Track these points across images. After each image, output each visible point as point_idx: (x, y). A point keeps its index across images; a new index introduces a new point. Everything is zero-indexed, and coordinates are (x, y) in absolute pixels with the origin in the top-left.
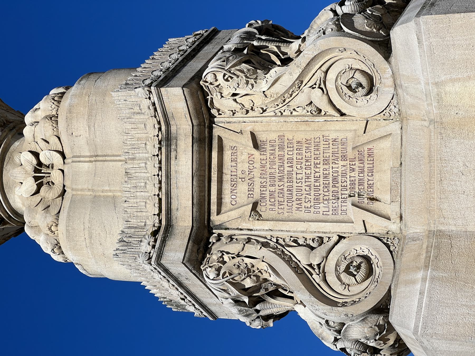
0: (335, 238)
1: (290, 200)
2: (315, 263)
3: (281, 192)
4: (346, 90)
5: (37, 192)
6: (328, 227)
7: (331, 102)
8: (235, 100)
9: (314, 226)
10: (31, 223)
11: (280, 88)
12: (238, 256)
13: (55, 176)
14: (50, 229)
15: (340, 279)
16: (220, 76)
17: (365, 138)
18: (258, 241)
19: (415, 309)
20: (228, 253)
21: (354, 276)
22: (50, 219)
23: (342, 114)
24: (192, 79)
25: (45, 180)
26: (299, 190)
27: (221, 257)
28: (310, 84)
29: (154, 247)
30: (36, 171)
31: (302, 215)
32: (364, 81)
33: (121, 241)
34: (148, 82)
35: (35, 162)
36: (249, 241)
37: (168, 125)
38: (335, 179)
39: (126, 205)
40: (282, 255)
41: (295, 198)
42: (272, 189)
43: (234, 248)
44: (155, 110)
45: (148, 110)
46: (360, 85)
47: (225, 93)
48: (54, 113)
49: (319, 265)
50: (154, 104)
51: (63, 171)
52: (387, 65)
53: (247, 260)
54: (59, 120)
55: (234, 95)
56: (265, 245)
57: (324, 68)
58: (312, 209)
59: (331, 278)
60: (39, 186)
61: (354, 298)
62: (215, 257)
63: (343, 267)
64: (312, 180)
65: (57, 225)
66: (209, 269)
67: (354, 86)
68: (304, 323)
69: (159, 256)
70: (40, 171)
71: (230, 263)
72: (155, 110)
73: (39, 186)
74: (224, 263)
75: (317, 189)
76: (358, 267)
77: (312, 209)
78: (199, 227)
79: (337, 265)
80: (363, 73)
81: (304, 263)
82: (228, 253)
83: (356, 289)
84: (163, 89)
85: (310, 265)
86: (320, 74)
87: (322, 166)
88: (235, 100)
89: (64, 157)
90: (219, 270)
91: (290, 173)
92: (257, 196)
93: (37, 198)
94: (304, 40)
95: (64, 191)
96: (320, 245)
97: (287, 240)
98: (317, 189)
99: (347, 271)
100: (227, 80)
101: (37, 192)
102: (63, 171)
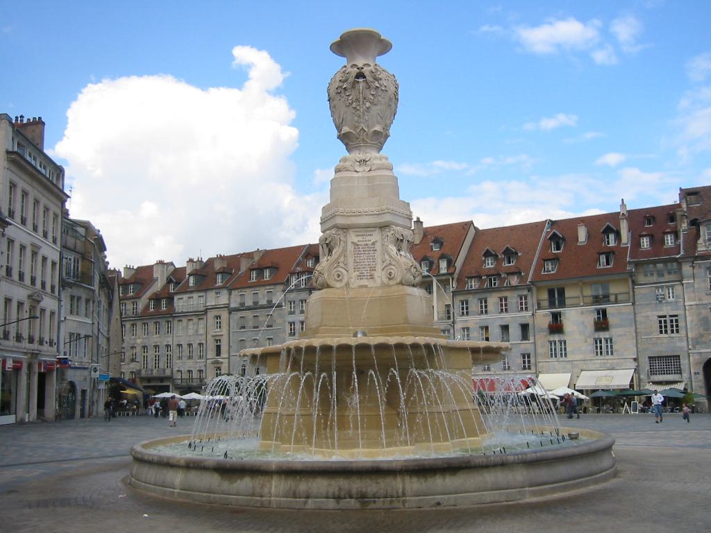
40: (342, 253)
79: (341, 272)
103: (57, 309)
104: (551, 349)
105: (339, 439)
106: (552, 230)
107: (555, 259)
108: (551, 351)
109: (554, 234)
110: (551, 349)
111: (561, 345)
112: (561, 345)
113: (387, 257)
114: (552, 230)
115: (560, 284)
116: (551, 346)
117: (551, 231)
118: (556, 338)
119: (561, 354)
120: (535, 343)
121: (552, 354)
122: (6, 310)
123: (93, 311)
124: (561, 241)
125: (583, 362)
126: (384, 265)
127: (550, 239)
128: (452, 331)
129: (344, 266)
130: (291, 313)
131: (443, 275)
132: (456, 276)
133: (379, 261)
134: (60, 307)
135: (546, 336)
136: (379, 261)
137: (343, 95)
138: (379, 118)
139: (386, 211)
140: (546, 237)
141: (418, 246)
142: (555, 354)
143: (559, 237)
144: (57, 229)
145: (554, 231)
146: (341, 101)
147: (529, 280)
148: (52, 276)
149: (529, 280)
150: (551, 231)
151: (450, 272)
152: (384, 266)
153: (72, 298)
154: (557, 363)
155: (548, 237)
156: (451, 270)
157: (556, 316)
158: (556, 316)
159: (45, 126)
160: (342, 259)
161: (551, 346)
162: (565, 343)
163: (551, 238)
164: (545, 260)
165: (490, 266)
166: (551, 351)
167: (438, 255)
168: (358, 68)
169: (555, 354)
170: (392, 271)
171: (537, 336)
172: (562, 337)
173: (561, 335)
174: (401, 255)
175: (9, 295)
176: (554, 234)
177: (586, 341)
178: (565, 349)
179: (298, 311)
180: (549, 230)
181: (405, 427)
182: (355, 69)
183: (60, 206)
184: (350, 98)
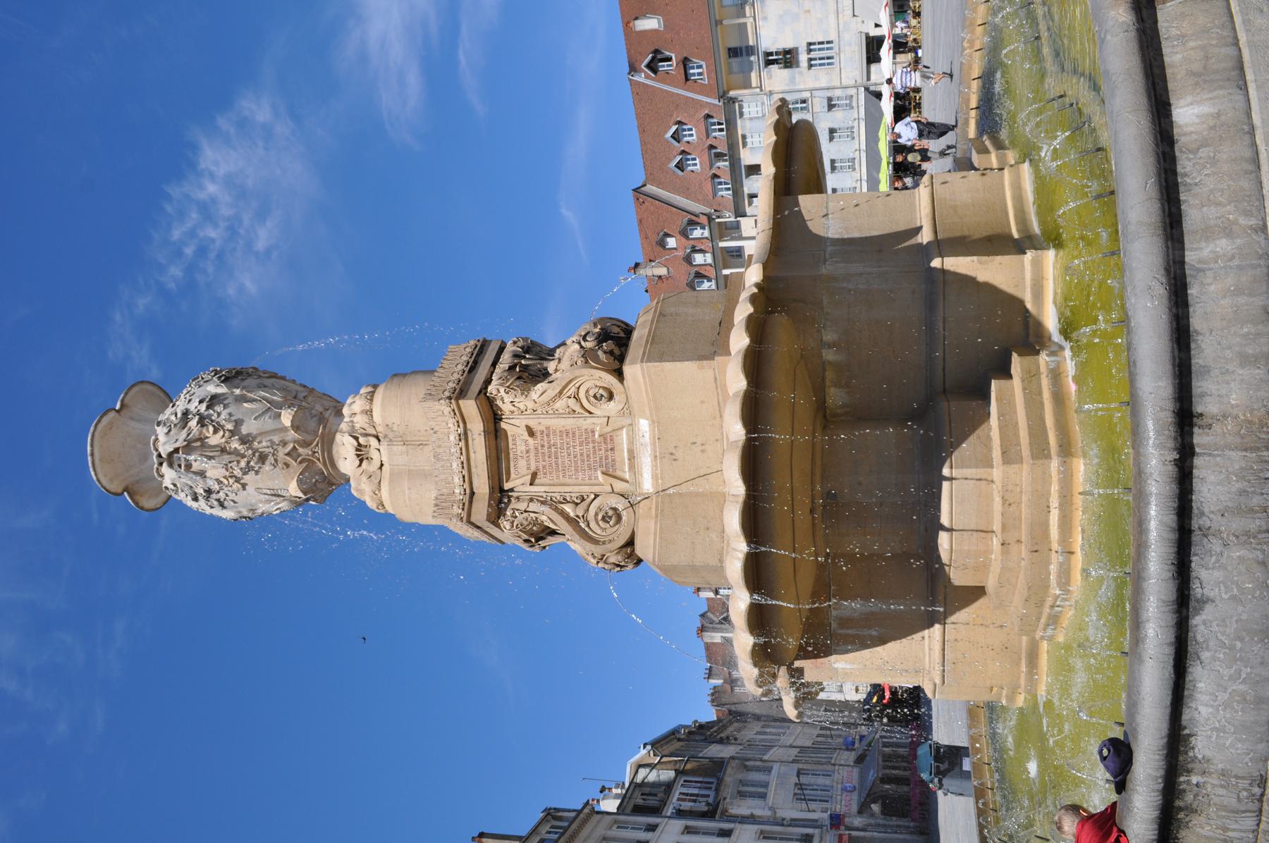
0: (593, 496)
1: (557, 470)
2: (581, 515)
3: (550, 465)
4: (592, 399)
5: (360, 465)
6: (586, 489)
7: (582, 406)
8: (514, 405)
9: (576, 489)
10: (860, 688)
11: (545, 398)
12: (526, 511)
13: (374, 454)
14: (374, 493)
15: (599, 525)
16: (502, 390)
17: (609, 429)
18: (538, 500)
19: (652, 542)
20: (517, 510)
21: (608, 522)
22: (374, 487)
23: (590, 413)
24: (480, 392)
25: (364, 456)
26: (563, 463)
27: (514, 512)
28: (568, 394)
29: (463, 509)
30: (357, 450)
31: (567, 480)
32: (605, 394)
33: (436, 505)
34: (447, 394)
35: (356, 444)
36: (531, 500)
37: (465, 423)
38: (588, 456)
39: (437, 479)
40: (556, 509)
41: (561, 469)
42: (544, 463)
43: (522, 506)
44: (455, 414)
45: (838, 810)
46: (602, 396)
47: (506, 400)
48: (368, 408)
49: (583, 516)
50: (454, 410)
51: (379, 450)
52: (620, 385)
53: (532, 515)
54: (374, 414)
55: (512, 402)
56: (543, 503)
57: (577, 385)
58: (574, 477)
59: (593, 525)
60: (361, 461)
61: (610, 538)
62: (509, 513)
63: (600, 517)
64: (572, 456)
65: (380, 490)
66: (505, 523)
67: (598, 396)
68: (575, 551)
69: (469, 515)
70: (360, 451)
71: (520, 517)
72: (455, 414)
73: (361, 461)
74: (516, 517)
75: (576, 462)
76: (610, 518)
77: (574, 477)
78: (586, 564)
79: (596, 514)
80: (604, 388)
81: (572, 514)
82: (517, 510)
83: (610, 531)
84: (460, 402)
85: (578, 516)
86: (573, 389)
87: (578, 448)
88: (514, 405)
89: (379, 440)
90: (513, 522)
91: (556, 452)
92: (533, 468)
93: (361, 469)
94: (560, 360)
95: (382, 465)
96: (582, 501)
97: (558, 498)
98: (576, 462)
99: (603, 518)
100: (507, 393)
101: (360, 465)
102: (379, 450)
103: (756, 827)
104: (820, 65)
106: (642, 71)
107: (685, 62)
108: (823, 64)
109: (649, 66)
110: (820, 65)
111: (815, 50)
112: (815, 50)
113: (560, 404)
114: (642, 71)
116: (816, 65)
117: (645, 72)
118: (803, 58)
119: (828, 49)
120: (811, 90)
121: (828, 64)
122: (776, 838)
123: (761, 760)
124: (659, 57)
125: (841, 16)
126: (578, 409)
129: (585, 504)
133: (569, 423)
134: (751, 819)
136: (569, 423)
137: (222, 495)
140: (652, 79)
141: (671, 269)
142: (828, 58)
144: (635, 823)
145: (643, 66)
146: (235, 499)
147: (716, 102)
148: (704, 833)
150: (645, 72)
152: (582, 411)
153: (742, 795)
154: (842, 55)
155: (653, 75)
156: (704, 220)
157: (770, 60)
158: (770, 60)
159: (485, 831)
160: (568, 509)
161: (816, 65)
162: (810, 44)
163: (655, 71)
164: (687, 79)
165: (697, 161)
166: (823, 64)
167: (684, 240)
168: (161, 464)
169: (828, 58)
170: (591, 393)
171: (802, 87)
173: (800, 49)
174: (556, 370)
176: (649, 66)
177: (808, 11)
178: (820, 43)
180: (643, 76)
181: (896, 10)
183: (600, 816)
184: (226, 482)
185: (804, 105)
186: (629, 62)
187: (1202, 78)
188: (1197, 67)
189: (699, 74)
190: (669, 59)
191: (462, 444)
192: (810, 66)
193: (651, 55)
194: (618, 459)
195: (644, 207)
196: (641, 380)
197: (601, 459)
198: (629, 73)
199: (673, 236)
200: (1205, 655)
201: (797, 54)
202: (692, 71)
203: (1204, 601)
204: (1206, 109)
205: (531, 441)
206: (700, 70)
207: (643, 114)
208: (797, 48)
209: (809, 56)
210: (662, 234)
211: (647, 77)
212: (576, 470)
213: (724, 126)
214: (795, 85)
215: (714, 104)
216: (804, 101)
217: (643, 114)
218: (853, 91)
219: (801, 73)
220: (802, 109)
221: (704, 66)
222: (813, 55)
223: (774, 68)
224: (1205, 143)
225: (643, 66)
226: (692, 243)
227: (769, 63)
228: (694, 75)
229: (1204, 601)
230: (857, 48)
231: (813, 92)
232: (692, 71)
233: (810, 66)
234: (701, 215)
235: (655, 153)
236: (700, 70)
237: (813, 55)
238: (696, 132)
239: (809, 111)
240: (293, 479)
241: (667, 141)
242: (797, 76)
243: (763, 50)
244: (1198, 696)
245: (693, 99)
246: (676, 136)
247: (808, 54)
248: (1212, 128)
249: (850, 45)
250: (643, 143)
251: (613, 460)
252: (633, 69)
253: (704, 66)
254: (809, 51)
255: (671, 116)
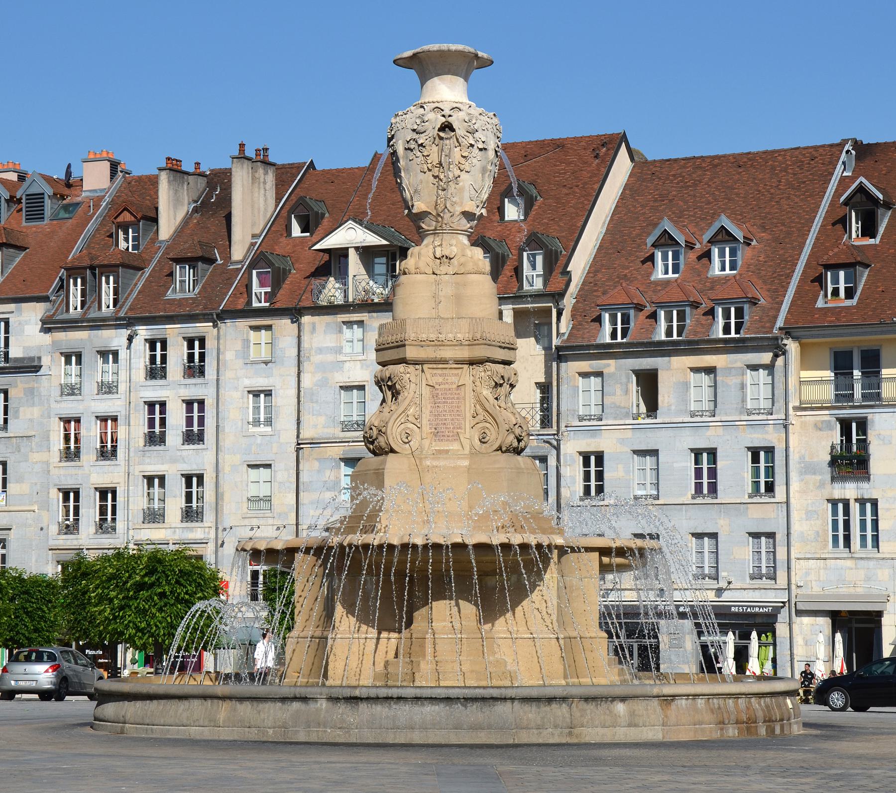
91: (447, 403)
105: (398, 675)
110: (835, 523)
112: (863, 512)
115: (868, 340)
116: (835, 513)
118: (850, 490)
119: (863, 538)
120: (787, 503)
121: (835, 538)
126: (476, 420)
127: (846, 203)
128: (552, 461)
130: (72, 391)
131: (537, 296)
132: (568, 301)
135: (822, 485)
138: (473, 192)
139: (481, 341)
140: (838, 194)
143: (874, 200)
147: (780, 323)
149: (780, 323)
150: (853, 179)
151: (552, 288)
154: (849, 563)
155: (842, 199)
156: (556, 284)
166: (835, 528)
170: (487, 431)
171: (794, 486)
172: (867, 490)
173: (865, 485)
175: (69, 483)
178: (875, 523)
179: (90, 387)
182: (439, 116)
185: (763, 489)
186: (877, 144)
187: (632, 714)
188: (636, 713)
189: (836, 292)
190: (869, 230)
191: (455, 343)
192: (834, 503)
193: (881, 197)
194: (442, 443)
195: (588, 155)
196: (497, 466)
197: (443, 432)
198: (857, 145)
199: (526, 214)
200: (448, 708)
201: (857, 479)
202: (842, 274)
203: (466, 707)
204: (622, 714)
205: (454, 386)
206: (842, 293)
207: (773, 168)
208: (869, 479)
209: (852, 503)
210: (534, 192)
211: (844, 182)
212: (435, 415)
213: (733, 335)
214: (801, 473)
215: (776, 317)
216: (770, 488)
217: (773, 168)
218: (782, 580)
219: (822, 485)
220: (756, 484)
221: (848, 303)
222: (855, 508)
223: (836, 437)
224: (611, 712)
225: (862, 179)
226: (512, 257)
227: (845, 425)
228: (836, 281)
229: (466, 707)
230: (860, 591)
231: (785, 506)
232: (842, 274)
233: (834, 503)
234: (566, 278)
235: (695, 185)
236: (842, 293)
237: (855, 508)
238: (727, 276)
239: (750, 497)
240: (428, 207)
241: (715, 216)
242: (818, 478)
243: (870, 417)
244: (433, 706)
245: (790, 276)
246: (723, 237)
247: (856, 500)
248: (616, 715)
249: (868, 579)
250: (716, 162)
251: (442, 440)
252: (863, 151)
253: (848, 303)
254: (862, 502)
255: (763, 228)
